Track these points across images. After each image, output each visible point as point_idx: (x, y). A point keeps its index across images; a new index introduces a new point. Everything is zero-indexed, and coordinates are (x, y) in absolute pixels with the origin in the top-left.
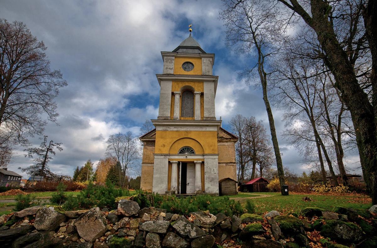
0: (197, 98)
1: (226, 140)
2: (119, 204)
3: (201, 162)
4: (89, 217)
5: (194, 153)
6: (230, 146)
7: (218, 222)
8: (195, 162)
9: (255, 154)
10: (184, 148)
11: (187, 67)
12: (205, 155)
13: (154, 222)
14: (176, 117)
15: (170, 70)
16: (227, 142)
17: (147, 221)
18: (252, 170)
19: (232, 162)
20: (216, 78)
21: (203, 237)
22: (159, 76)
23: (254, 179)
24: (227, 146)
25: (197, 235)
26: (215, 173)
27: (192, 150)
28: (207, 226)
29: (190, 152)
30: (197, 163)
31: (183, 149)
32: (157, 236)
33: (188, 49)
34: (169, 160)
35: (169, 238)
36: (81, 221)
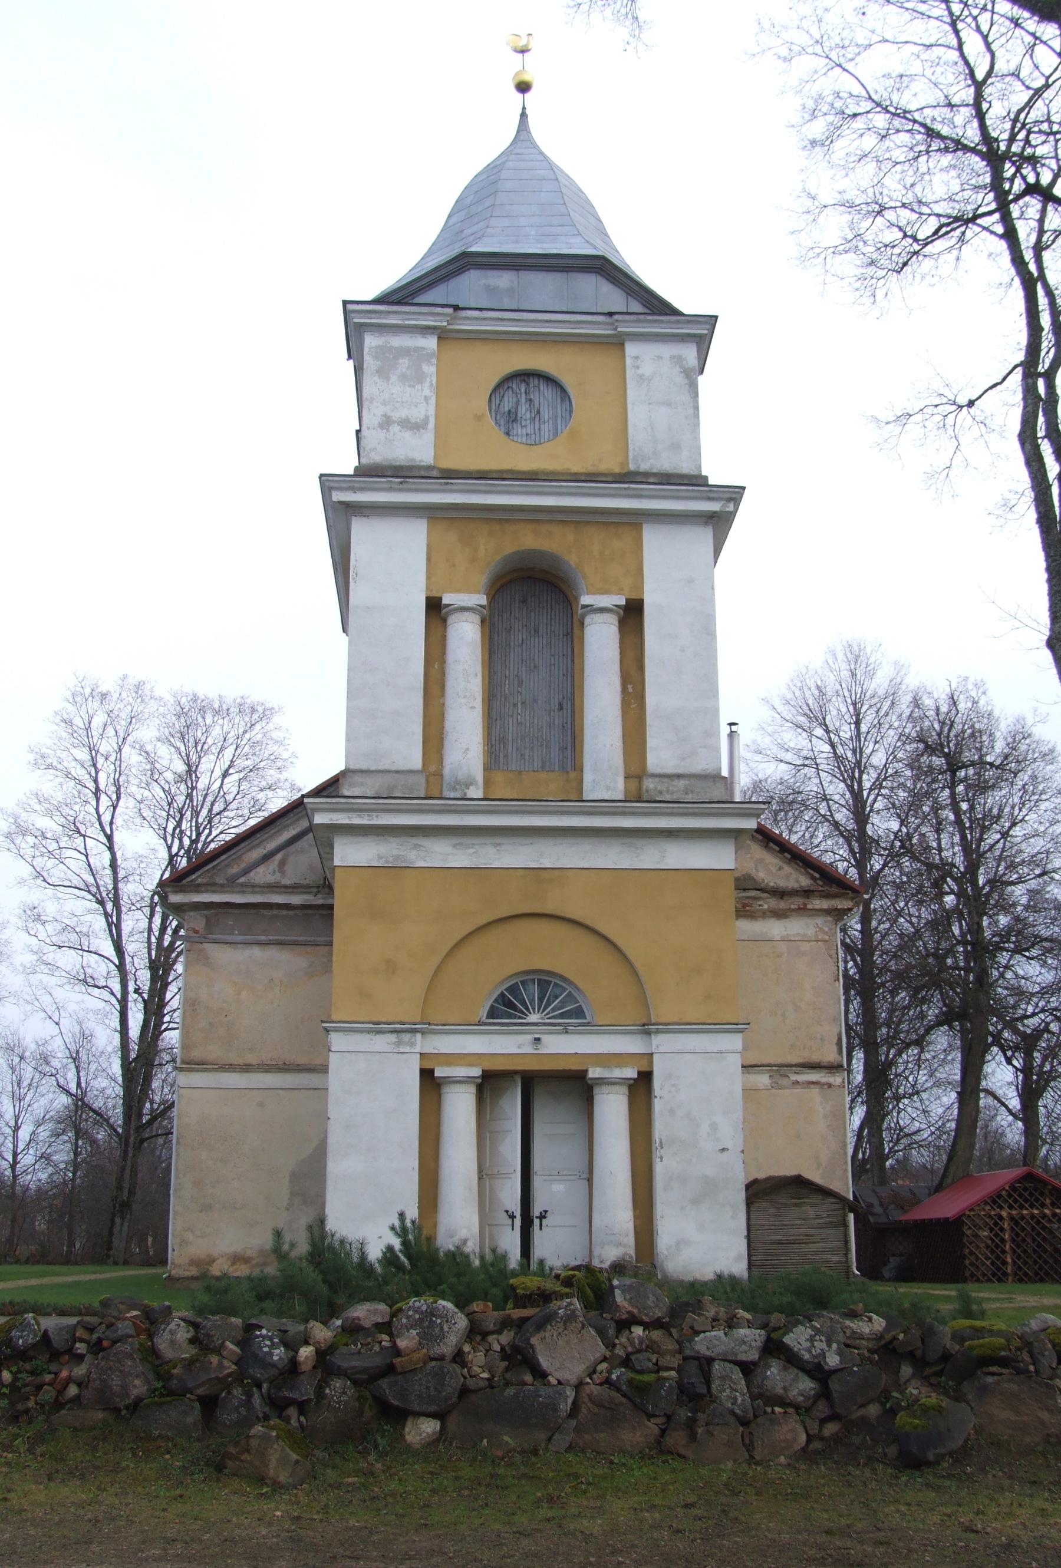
0: (601, 638)
1: (772, 903)
2: (617, 1292)
3: (631, 1073)
4: (565, 1323)
5: (579, 1013)
6: (805, 947)
7: (888, 1337)
8: (594, 1073)
9: (983, 982)
10: (518, 980)
11: (523, 410)
12: (658, 1032)
13: (725, 1334)
14: (461, 775)
15: (407, 434)
16: (779, 915)
17: (704, 1332)
18: (951, 1097)
19: (815, 1058)
20: (730, 500)
21: (855, 1369)
22: (340, 489)
23: (968, 1176)
24: (783, 947)
25: (841, 1362)
26: (723, 1150)
27: (570, 995)
28: (864, 1342)
29: (553, 1010)
30: (602, 1081)
31: (513, 989)
32: (736, 1369)
33: (522, 274)
34: (428, 1065)
35: (769, 1373)
36: (547, 1334)
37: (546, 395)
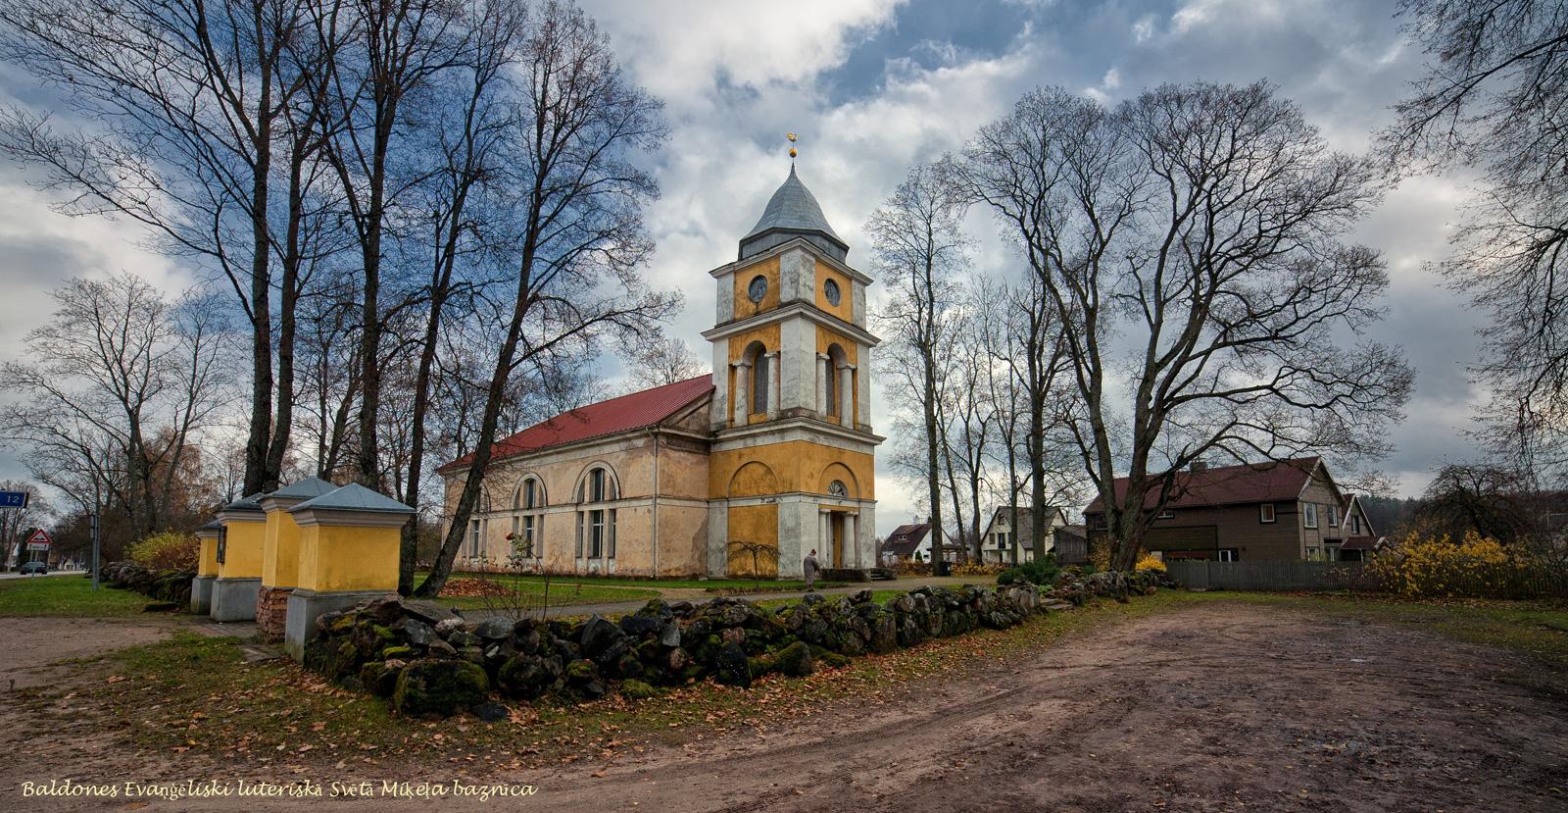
37: (833, 289)
